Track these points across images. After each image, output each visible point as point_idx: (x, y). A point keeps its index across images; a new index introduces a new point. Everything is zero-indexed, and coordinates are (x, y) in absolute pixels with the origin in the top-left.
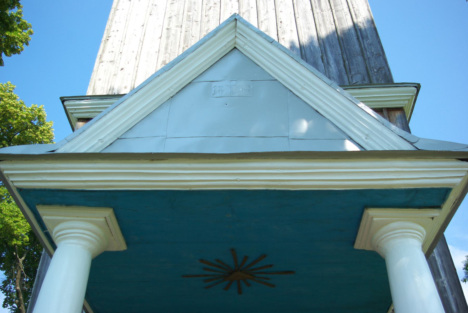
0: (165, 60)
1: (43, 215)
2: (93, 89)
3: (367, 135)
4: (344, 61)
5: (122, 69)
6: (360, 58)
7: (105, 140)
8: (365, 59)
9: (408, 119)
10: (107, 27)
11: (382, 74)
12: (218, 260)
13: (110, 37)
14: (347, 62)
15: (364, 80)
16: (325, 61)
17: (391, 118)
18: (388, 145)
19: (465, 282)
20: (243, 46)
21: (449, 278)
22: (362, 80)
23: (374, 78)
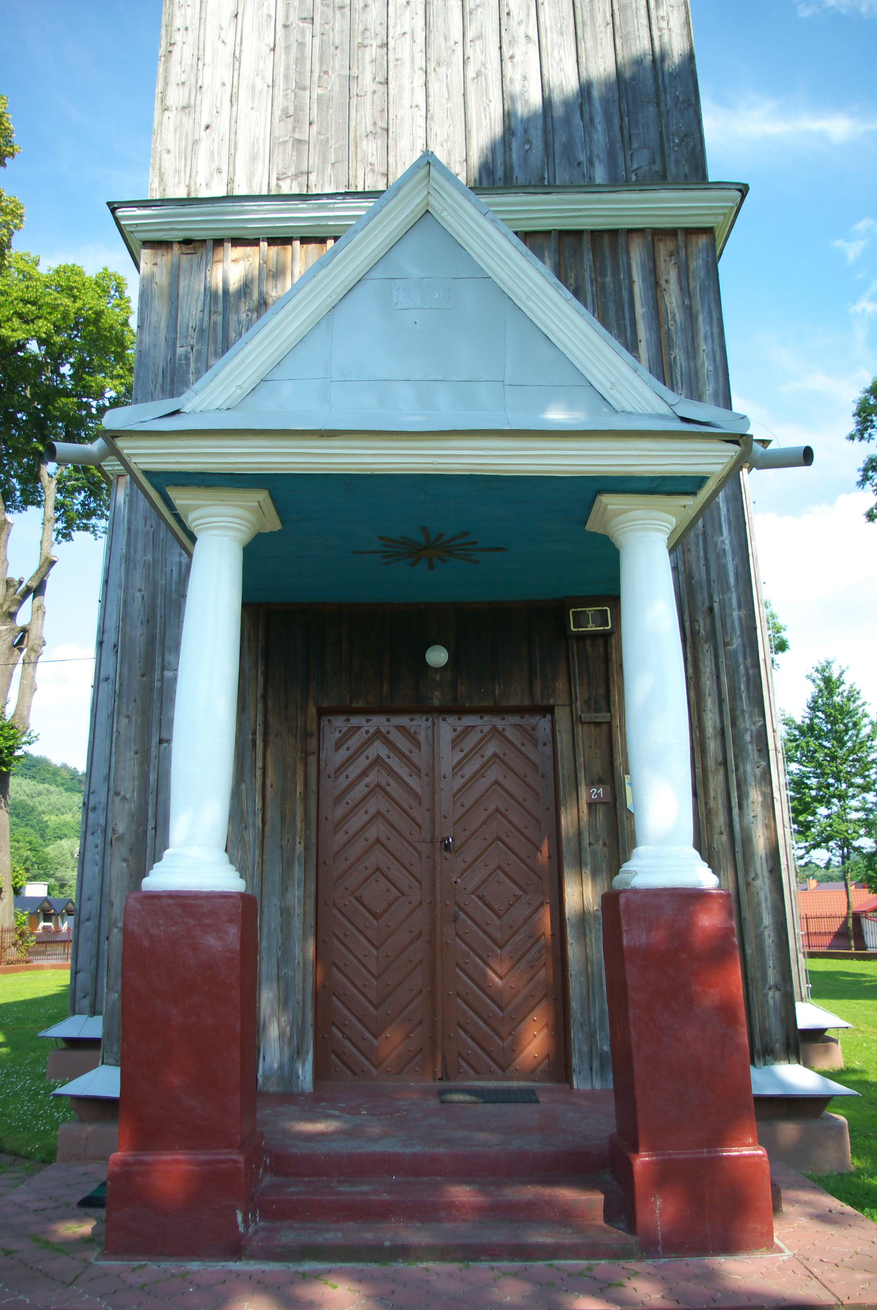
0: (287, 108)
1: (176, 499)
2: (160, 174)
3: (613, 384)
4: (622, 118)
5: (207, 127)
6: (651, 111)
7: (245, 386)
8: (660, 114)
9: (718, 253)
10: (165, 20)
11: (688, 148)
12: (403, 538)
13: (174, 44)
14: (626, 119)
15: (654, 162)
16: (587, 116)
17: (690, 249)
18: (639, 402)
19: (851, 441)
20: (439, 212)
21: (733, 537)
22: (649, 164)
23: (673, 158)
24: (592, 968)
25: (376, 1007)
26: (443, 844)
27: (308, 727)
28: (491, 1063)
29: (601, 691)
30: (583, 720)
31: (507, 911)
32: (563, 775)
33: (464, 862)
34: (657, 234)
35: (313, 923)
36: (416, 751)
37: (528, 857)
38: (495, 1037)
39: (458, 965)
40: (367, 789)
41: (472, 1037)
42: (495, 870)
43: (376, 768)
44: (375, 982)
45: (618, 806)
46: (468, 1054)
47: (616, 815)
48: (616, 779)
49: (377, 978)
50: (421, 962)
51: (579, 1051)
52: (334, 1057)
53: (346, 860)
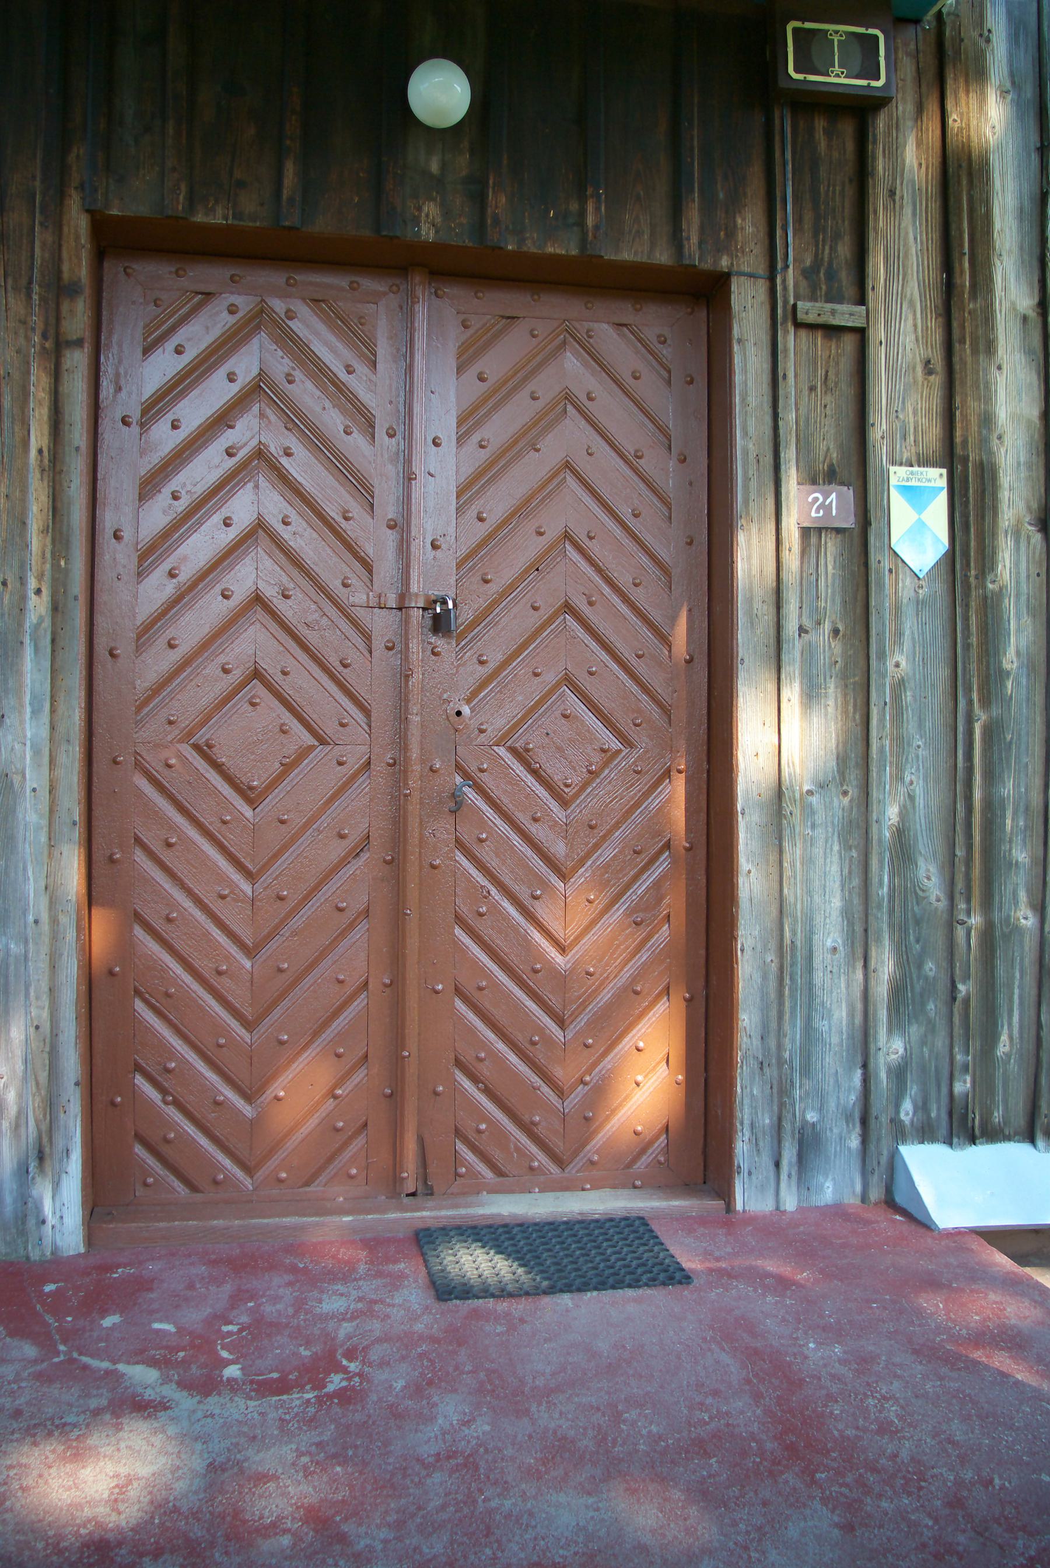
24: (794, 932)
25: (249, 1025)
26: (429, 615)
27: (65, 268)
28: (534, 1149)
29: (845, 250)
30: (801, 316)
31: (583, 788)
32: (746, 452)
33: (482, 663)
35: (77, 813)
36: (361, 369)
37: (639, 657)
38: (546, 1089)
39: (459, 920)
40: (230, 463)
41: (488, 1092)
42: (557, 686)
43: (256, 408)
44: (248, 964)
45: (872, 539)
46: (479, 1132)
47: (866, 565)
48: (871, 474)
49: (249, 952)
50: (366, 913)
51: (752, 1126)
52: (139, 1150)
53: (172, 646)
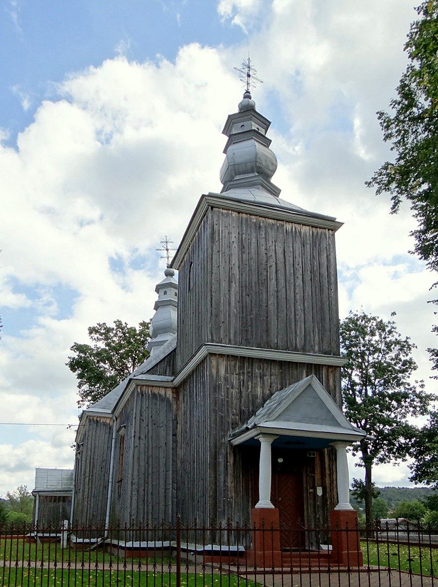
34: (329, 367)
